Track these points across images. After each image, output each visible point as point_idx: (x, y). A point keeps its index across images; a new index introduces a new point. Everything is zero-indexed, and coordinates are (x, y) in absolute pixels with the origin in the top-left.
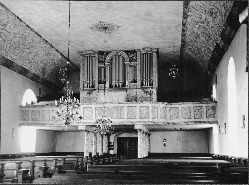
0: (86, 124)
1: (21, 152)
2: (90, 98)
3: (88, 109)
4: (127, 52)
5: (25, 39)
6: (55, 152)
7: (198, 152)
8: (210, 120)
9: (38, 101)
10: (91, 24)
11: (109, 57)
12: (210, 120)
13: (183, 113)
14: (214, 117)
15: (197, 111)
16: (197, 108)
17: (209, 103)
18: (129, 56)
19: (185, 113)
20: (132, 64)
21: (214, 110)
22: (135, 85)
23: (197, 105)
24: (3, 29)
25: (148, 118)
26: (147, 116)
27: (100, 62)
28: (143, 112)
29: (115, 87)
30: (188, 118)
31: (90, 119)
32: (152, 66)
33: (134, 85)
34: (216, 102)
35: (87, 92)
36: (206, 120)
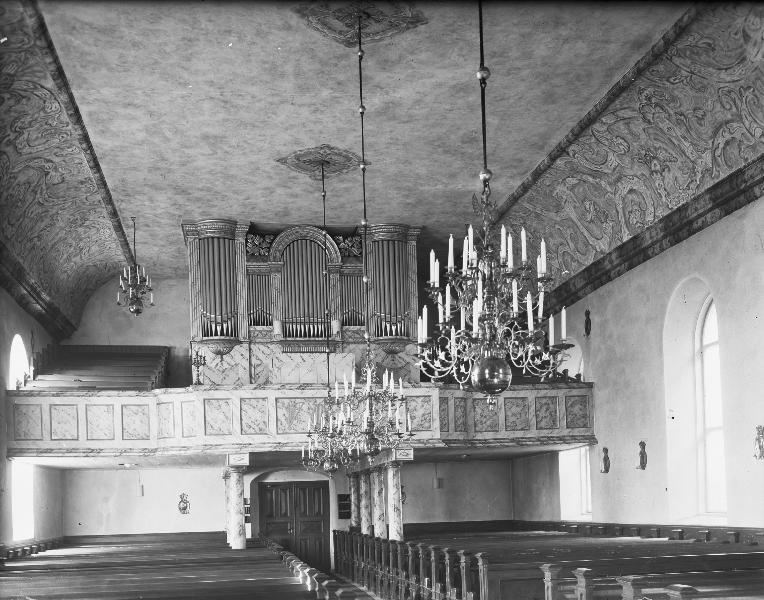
0: (251, 450)
1: (562, 519)
2: (226, 366)
3: (254, 402)
4: (333, 233)
5: (47, 174)
6: (555, 520)
7: (490, 519)
8: (576, 432)
9: (36, 374)
10: (286, 150)
11: (279, 244)
12: (576, 432)
13: (509, 413)
14: (585, 426)
15: (544, 408)
16: (544, 401)
17: (574, 388)
18: (338, 244)
19: (514, 415)
20: (349, 267)
21: (585, 406)
22: (357, 332)
23: (543, 393)
24: (10, 143)
25: (428, 429)
26: (427, 425)
27: (251, 257)
28: (416, 414)
29: (301, 336)
30: (522, 429)
31: (262, 432)
32: (406, 276)
33: (353, 332)
34: (590, 385)
35: (214, 347)
36: (566, 432)
